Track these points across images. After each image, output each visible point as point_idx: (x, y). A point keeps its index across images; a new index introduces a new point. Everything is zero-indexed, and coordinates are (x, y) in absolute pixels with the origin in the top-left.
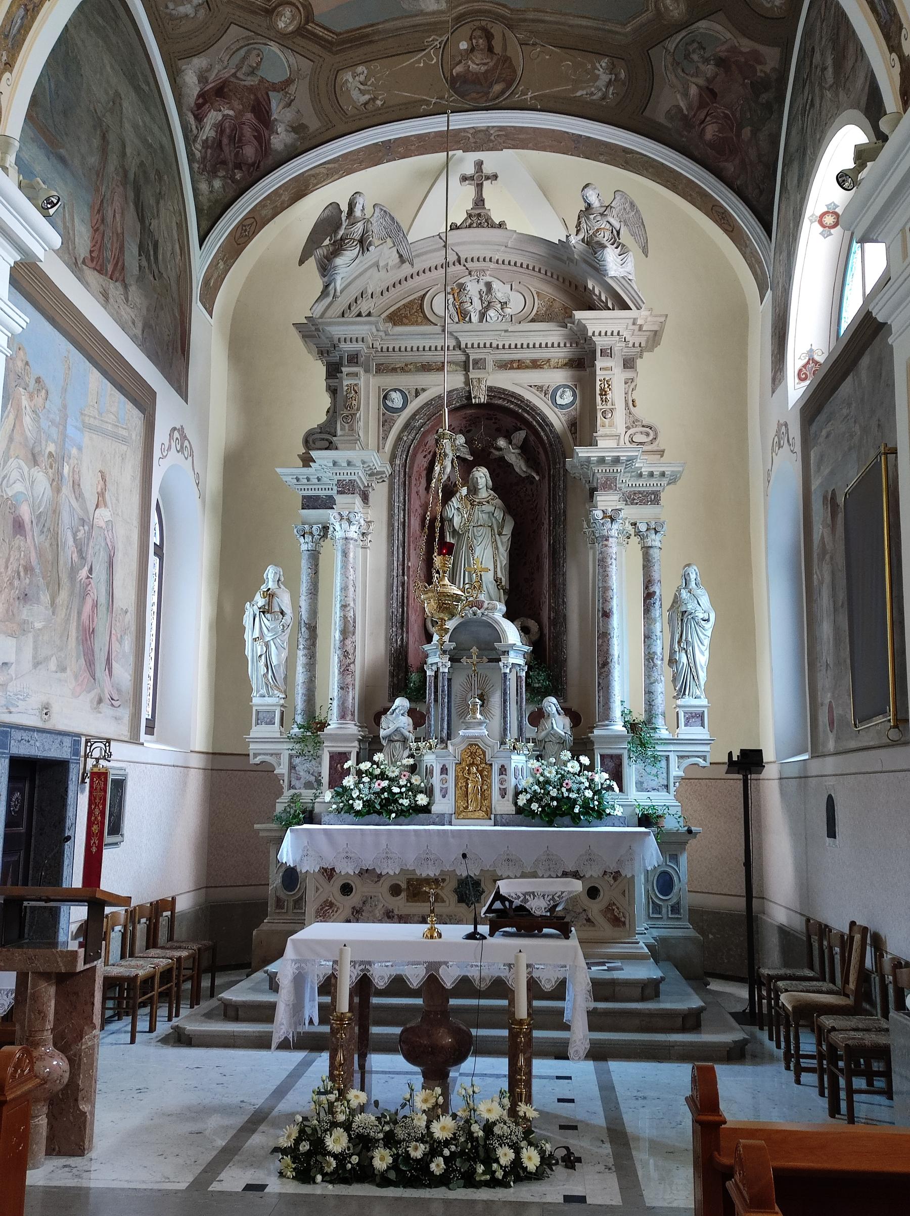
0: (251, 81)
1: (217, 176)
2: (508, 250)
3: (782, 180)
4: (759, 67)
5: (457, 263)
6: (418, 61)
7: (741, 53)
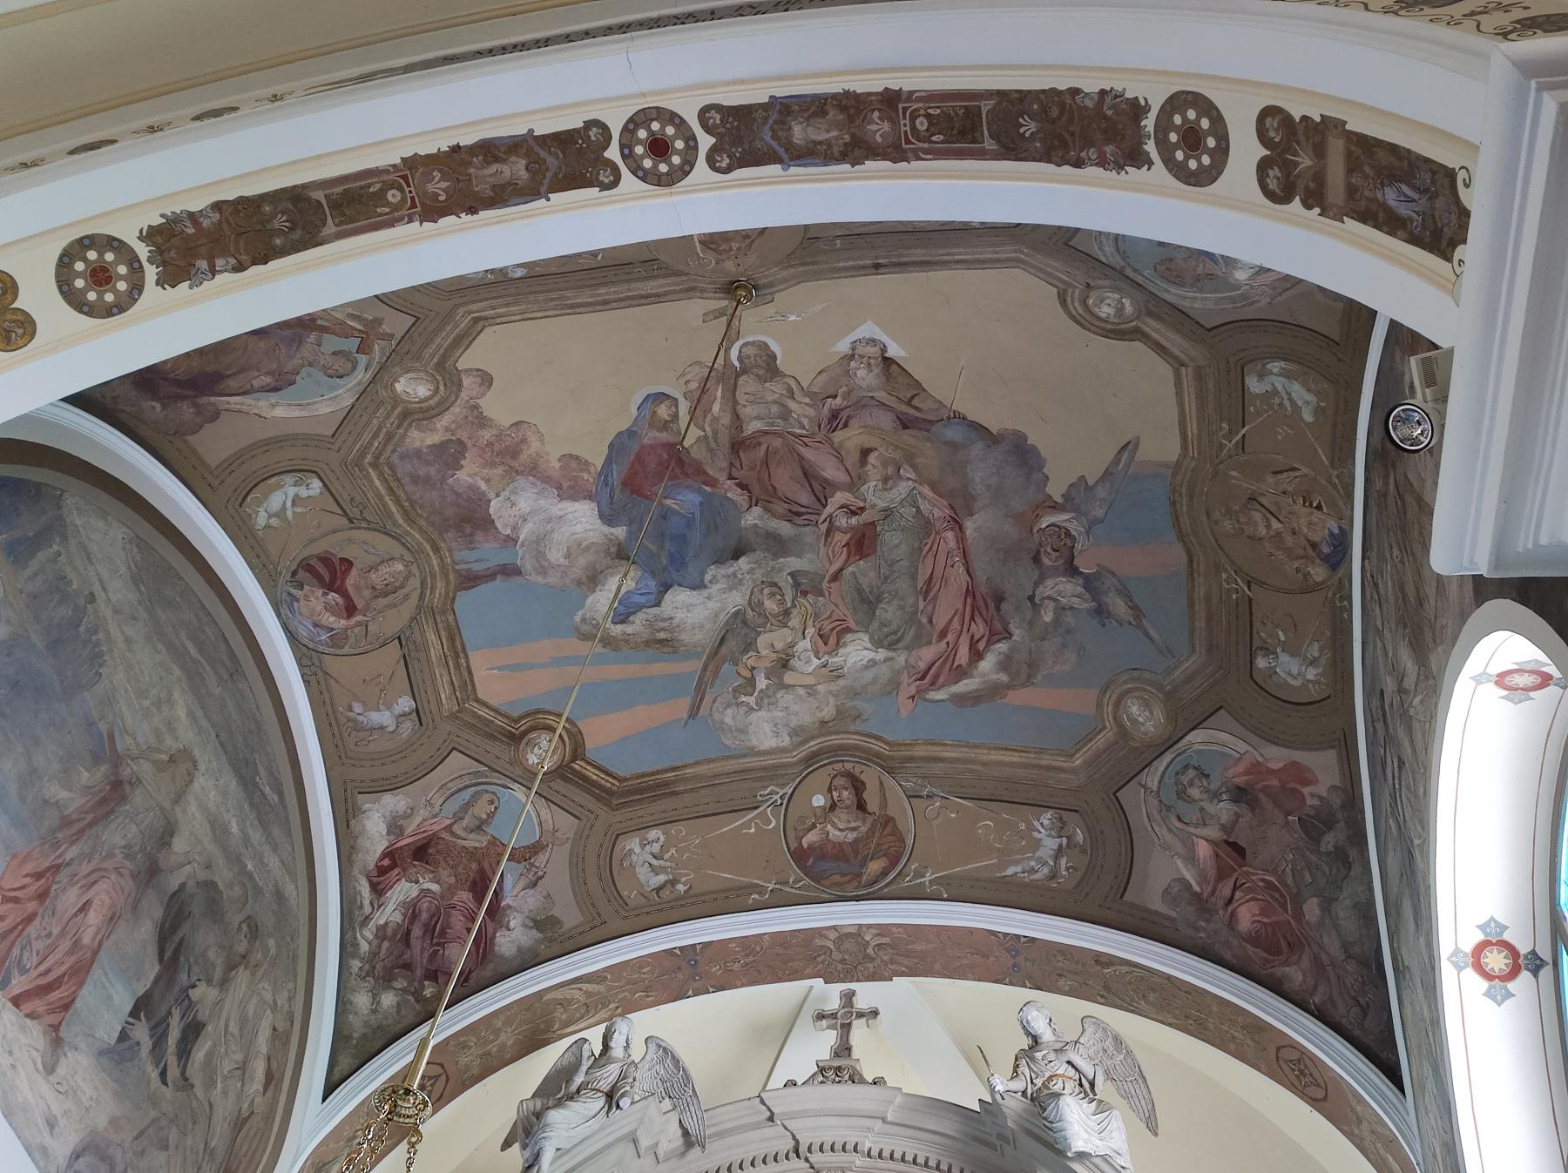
0: (475, 841)
1: (391, 988)
2: (888, 1128)
3: (1392, 947)
4: (1306, 790)
5: (792, 1155)
6: (747, 825)
7: (1272, 772)
